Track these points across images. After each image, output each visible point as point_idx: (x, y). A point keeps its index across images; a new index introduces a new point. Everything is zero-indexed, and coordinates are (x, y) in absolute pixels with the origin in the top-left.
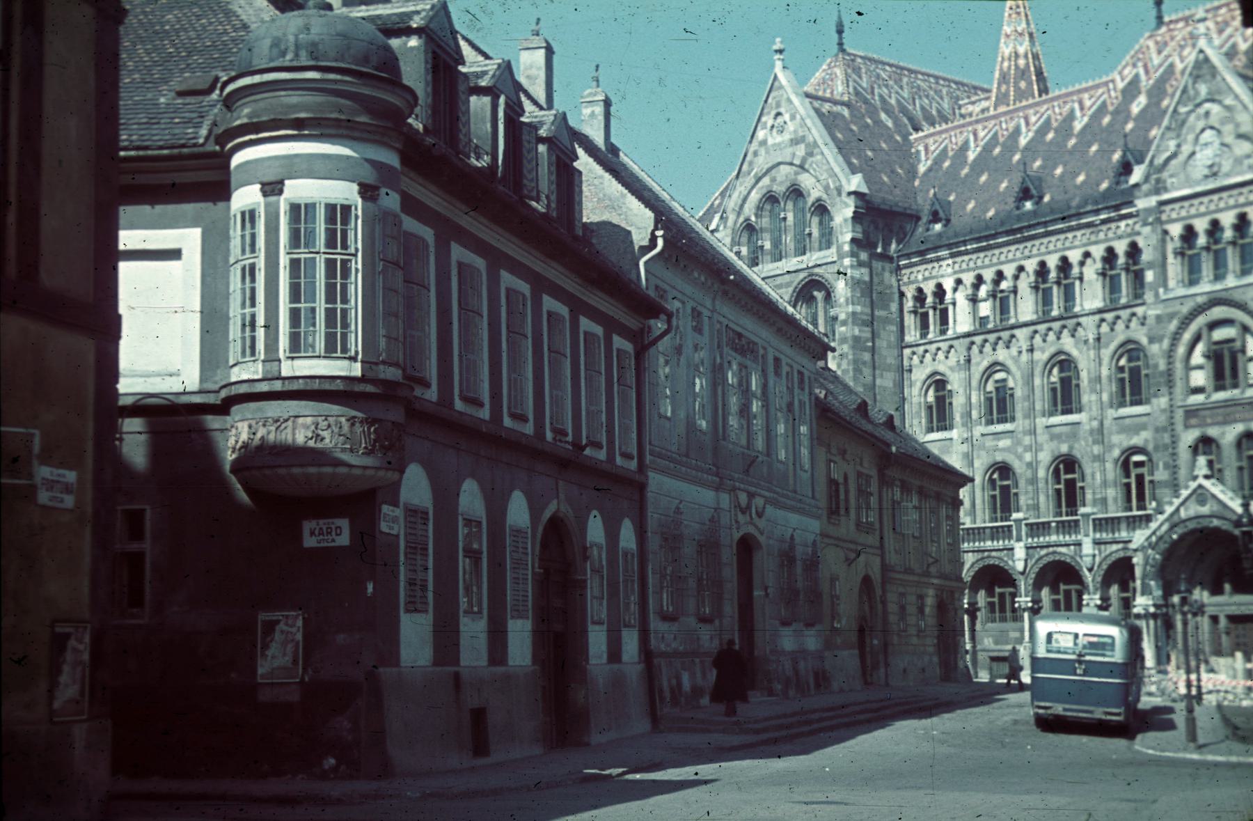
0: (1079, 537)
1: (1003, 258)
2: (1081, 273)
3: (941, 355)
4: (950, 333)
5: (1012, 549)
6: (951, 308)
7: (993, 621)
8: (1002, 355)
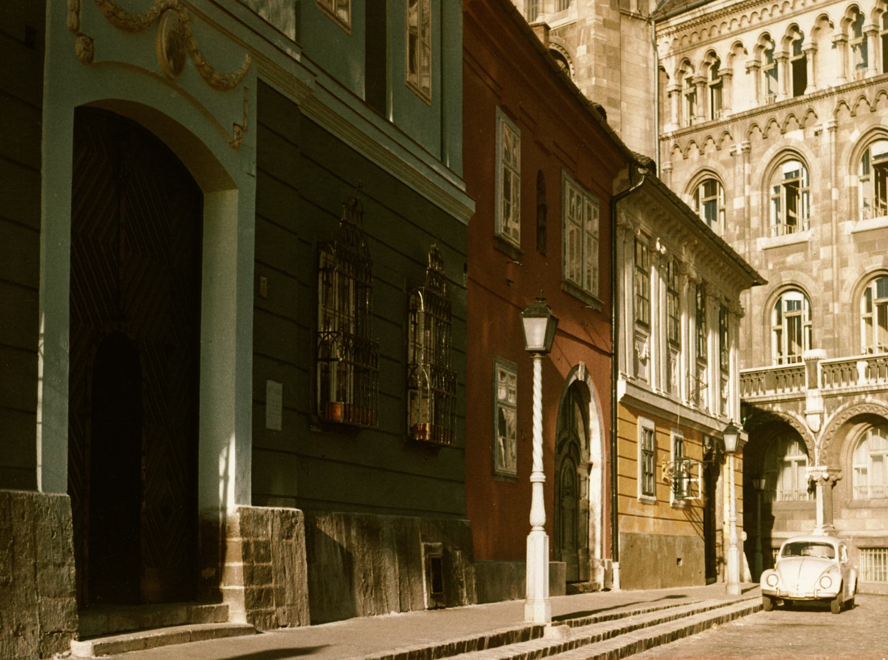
0: (803, 389)
1: (745, 24)
2: (815, 44)
3: (711, 148)
4: (809, 91)
5: (803, 399)
6: (810, 57)
7: (281, 592)
8: (795, 137)
